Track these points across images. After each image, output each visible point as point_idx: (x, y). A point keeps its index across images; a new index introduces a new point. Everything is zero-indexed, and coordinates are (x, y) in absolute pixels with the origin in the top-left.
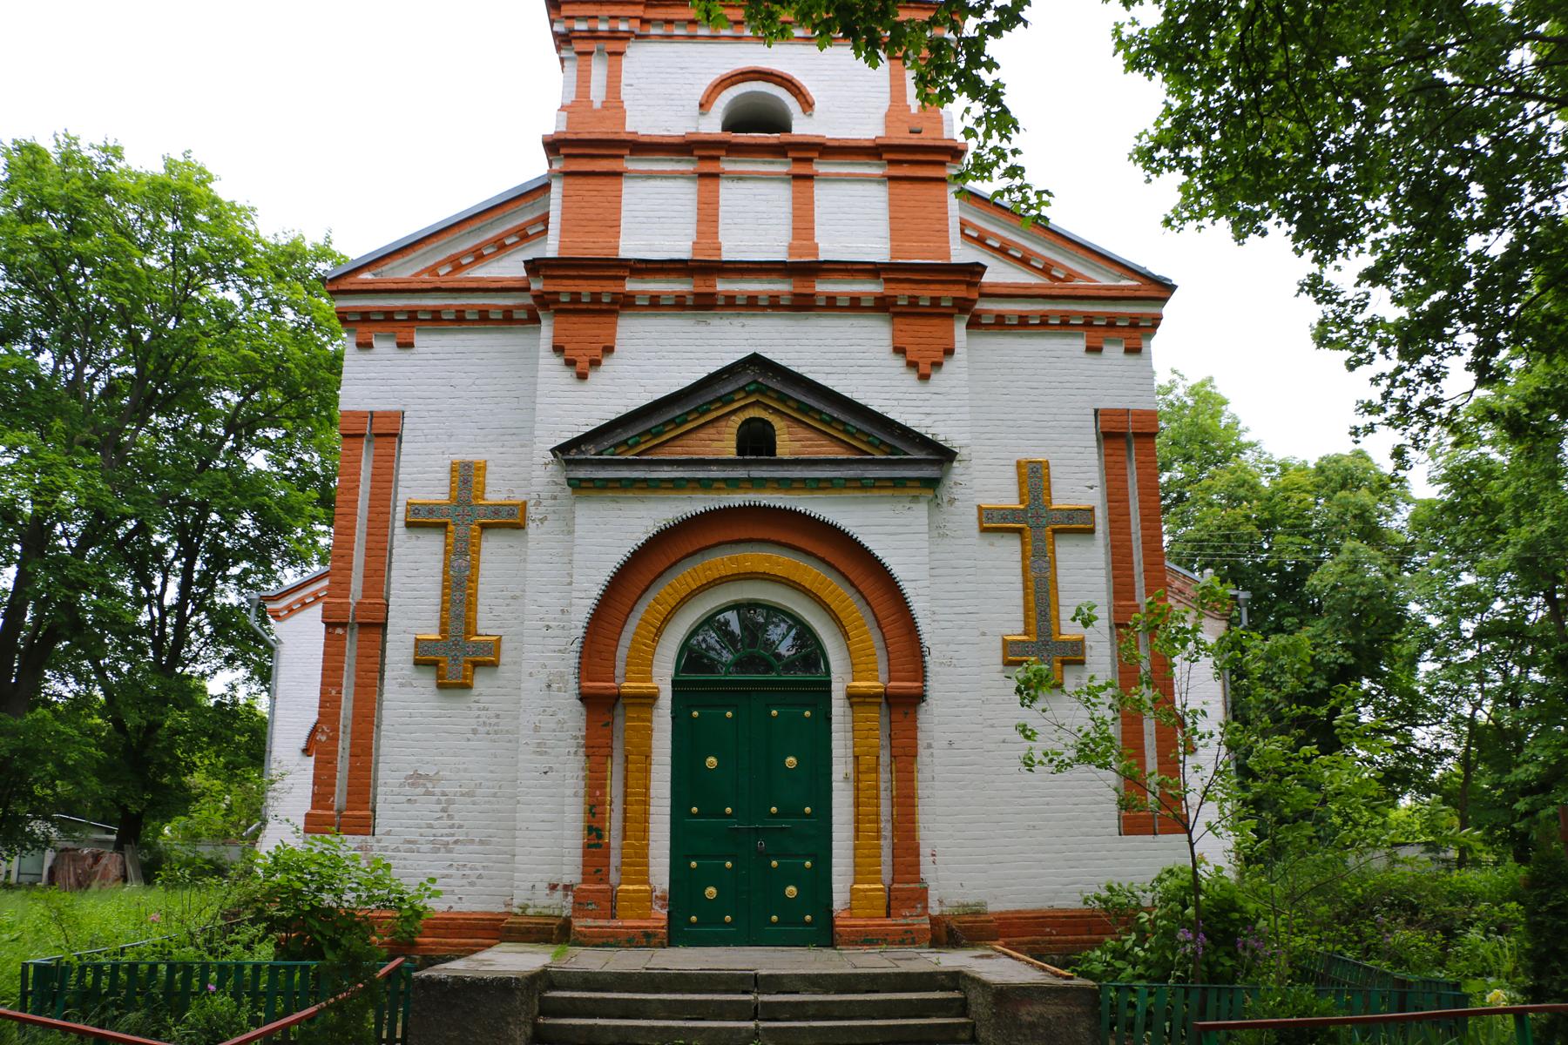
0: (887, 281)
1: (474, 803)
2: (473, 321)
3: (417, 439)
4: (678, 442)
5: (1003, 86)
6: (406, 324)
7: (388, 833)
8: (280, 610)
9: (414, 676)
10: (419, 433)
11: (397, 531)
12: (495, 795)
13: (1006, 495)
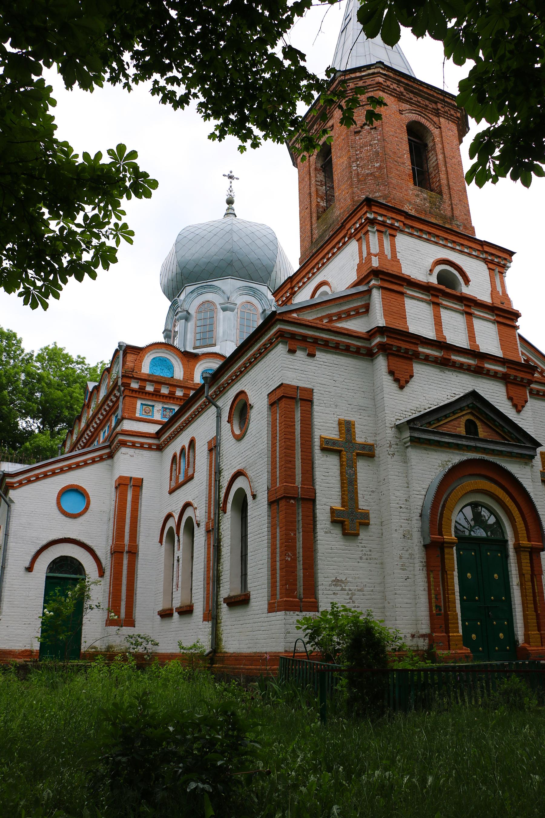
0: (508, 367)
2: (342, 350)
4: (445, 426)
6: (312, 344)
8: (15, 483)
9: (332, 528)
10: (322, 402)
11: (316, 451)
12: (372, 591)
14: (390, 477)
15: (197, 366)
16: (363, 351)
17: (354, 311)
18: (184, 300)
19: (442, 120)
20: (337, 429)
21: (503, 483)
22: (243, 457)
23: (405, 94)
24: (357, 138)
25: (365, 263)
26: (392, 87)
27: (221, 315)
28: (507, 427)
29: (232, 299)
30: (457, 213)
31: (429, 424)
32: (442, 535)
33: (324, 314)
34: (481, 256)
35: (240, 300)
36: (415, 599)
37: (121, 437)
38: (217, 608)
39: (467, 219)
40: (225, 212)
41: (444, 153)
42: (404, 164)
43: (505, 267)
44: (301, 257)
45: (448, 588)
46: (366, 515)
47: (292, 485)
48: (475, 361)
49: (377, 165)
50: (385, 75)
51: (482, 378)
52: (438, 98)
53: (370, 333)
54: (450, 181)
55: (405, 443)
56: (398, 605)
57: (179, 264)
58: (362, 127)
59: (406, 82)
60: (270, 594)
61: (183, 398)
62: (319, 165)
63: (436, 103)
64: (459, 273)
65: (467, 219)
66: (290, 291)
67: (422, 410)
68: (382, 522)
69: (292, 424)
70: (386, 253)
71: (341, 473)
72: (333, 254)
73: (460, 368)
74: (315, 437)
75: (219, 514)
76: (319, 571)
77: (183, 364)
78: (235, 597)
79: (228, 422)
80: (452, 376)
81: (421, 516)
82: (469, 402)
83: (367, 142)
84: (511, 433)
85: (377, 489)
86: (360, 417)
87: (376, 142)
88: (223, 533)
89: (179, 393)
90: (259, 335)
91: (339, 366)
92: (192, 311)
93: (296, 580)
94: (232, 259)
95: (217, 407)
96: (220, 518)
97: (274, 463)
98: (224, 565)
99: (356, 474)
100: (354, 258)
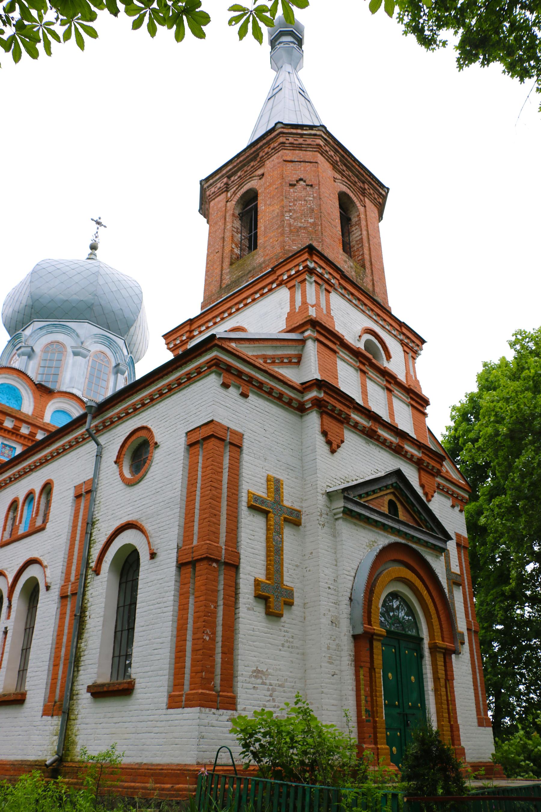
0: (423, 453)
1: (284, 692)
3: (250, 454)
5: (466, 393)
9: (255, 604)
10: (251, 451)
14: (320, 550)
15: (50, 404)
16: (294, 404)
17: (287, 358)
18: (31, 336)
19: (366, 200)
20: (265, 486)
21: (422, 574)
22: (134, 507)
23: (339, 164)
24: (292, 190)
25: (298, 312)
26: (329, 153)
27: (70, 359)
28: (424, 515)
29: (87, 345)
31: (360, 496)
32: (371, 625)
33: (260, 353)
34: (399, 337)
35: (95, 348)
36: (341, 700)
38: (71, 699)
40: (87, 256)
42: (336, 227)
43: (416, 353)
45: (376, 689)
46: (290, 593)
47: (216, 545)
48: (396, 439)
50: (325, 140)
51: (400, 459)
52: (366, 179)
53: (304, 386)
55: (335, 514)
56: (325, 707)
57: (31, 296)
58: (297, 181)
59: (342, 153)
60: (172, 684)
61: (28, 436)
62: (237, 212)
63: (363, 183)
66: (188, 334)
67: (350, 481)
68: (305, 604)
69: (220, 470)
71: (268, 539)
72: (254, 300)
73: (383, 443)
74: (243, 491)
75: (86, 576)
76: (240, 657)
77: (35, 398)
78: (103, 685)
79: (116, 462)
80: (375, 451)
81: (351, 599)
83: (301, 196)
84: (427, 522)
85: (301, 563)
86: (288, 477)
87: (311, 199)
88: (90, 600)
89: (25, 430)
90: (184, 361)
91: (270, 415)
92: (38, 349)
93: (213, 667)
94: (93, 302)
95: (98, 444)
96: (88, 581)
97: (190, 515)
98: (90, 642)
99: (282, 542)
100: (282, 307)
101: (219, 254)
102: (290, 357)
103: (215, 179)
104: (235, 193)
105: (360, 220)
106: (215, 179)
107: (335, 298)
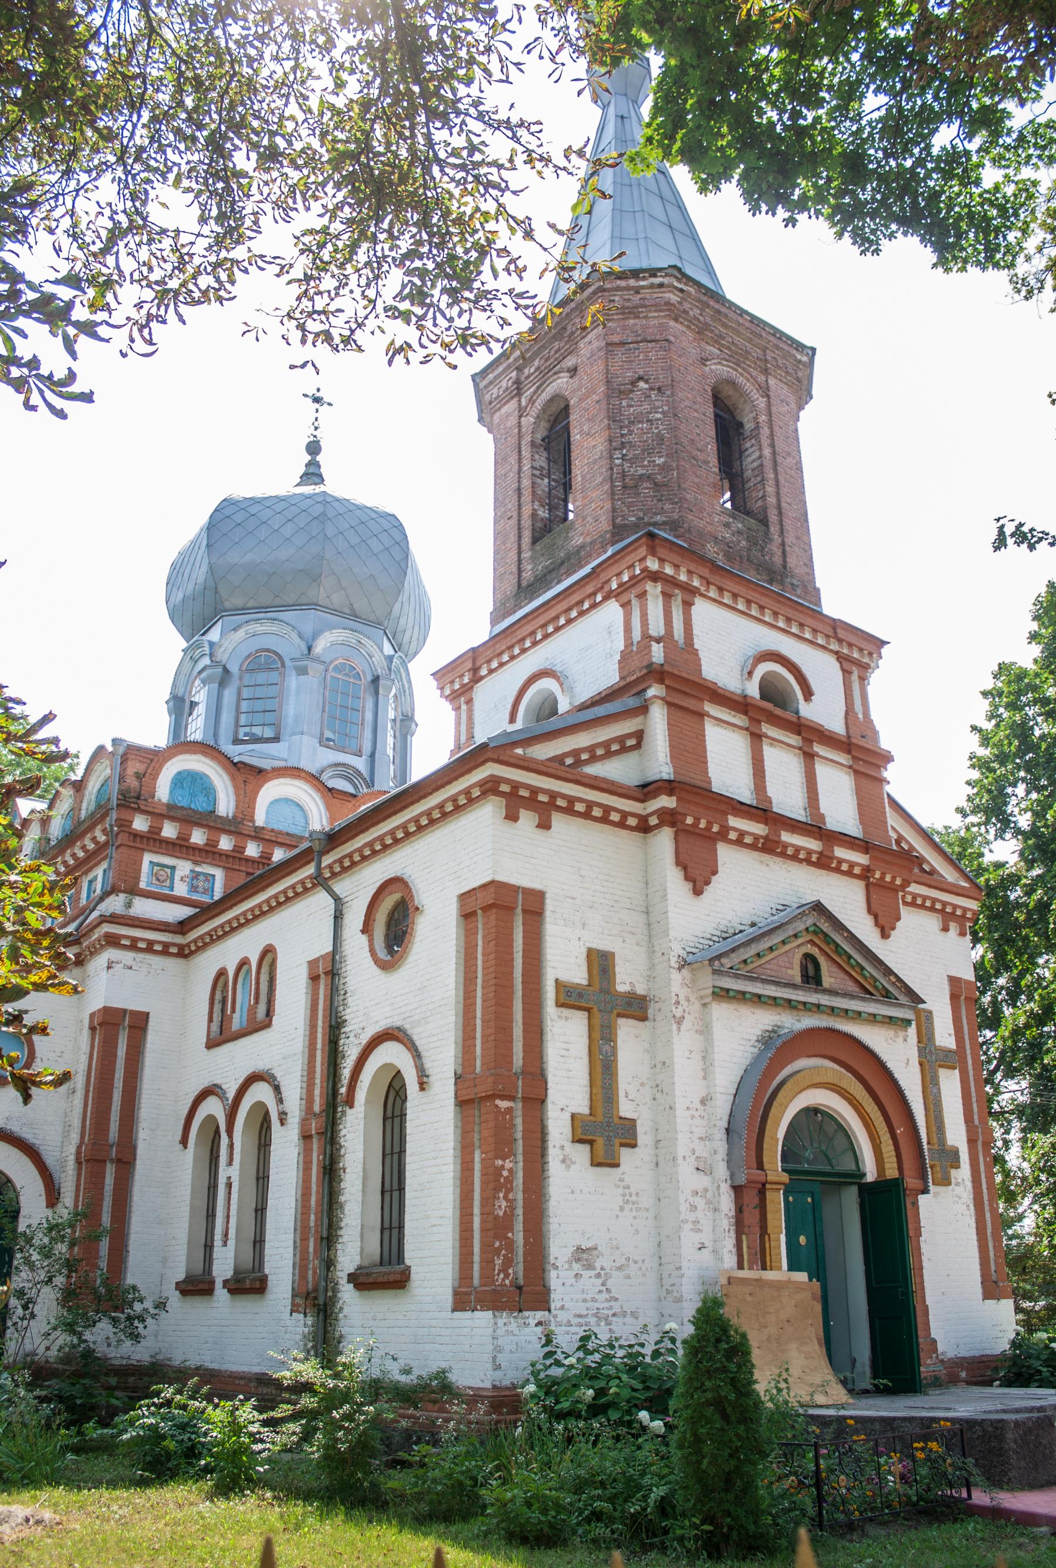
7: (562, 1308)
13: (577, 974)
25: (638, 652)
30: (791, 561)
37: (106, 928)
39: (808, 574)
41: (772, 445)
42: (707, 463)
44: (495, 610)
49: (660, 461)
50: (682, 291)
53: (646, 790)
54: (783, 500)
58: (633, 383)
62: (539, 436)
64: (796, 678)
65: (808, 574)
70: (676, 637)
79: (363, 932)
81: (728, 1130)
82: (810, 921)
87: (659, 416)
101: (514, 521)
102: (621, 739)
103: (496, 372)
104: (531, 401)
105: (757, 427)
106: (496, 372)
107: (703, 611)
